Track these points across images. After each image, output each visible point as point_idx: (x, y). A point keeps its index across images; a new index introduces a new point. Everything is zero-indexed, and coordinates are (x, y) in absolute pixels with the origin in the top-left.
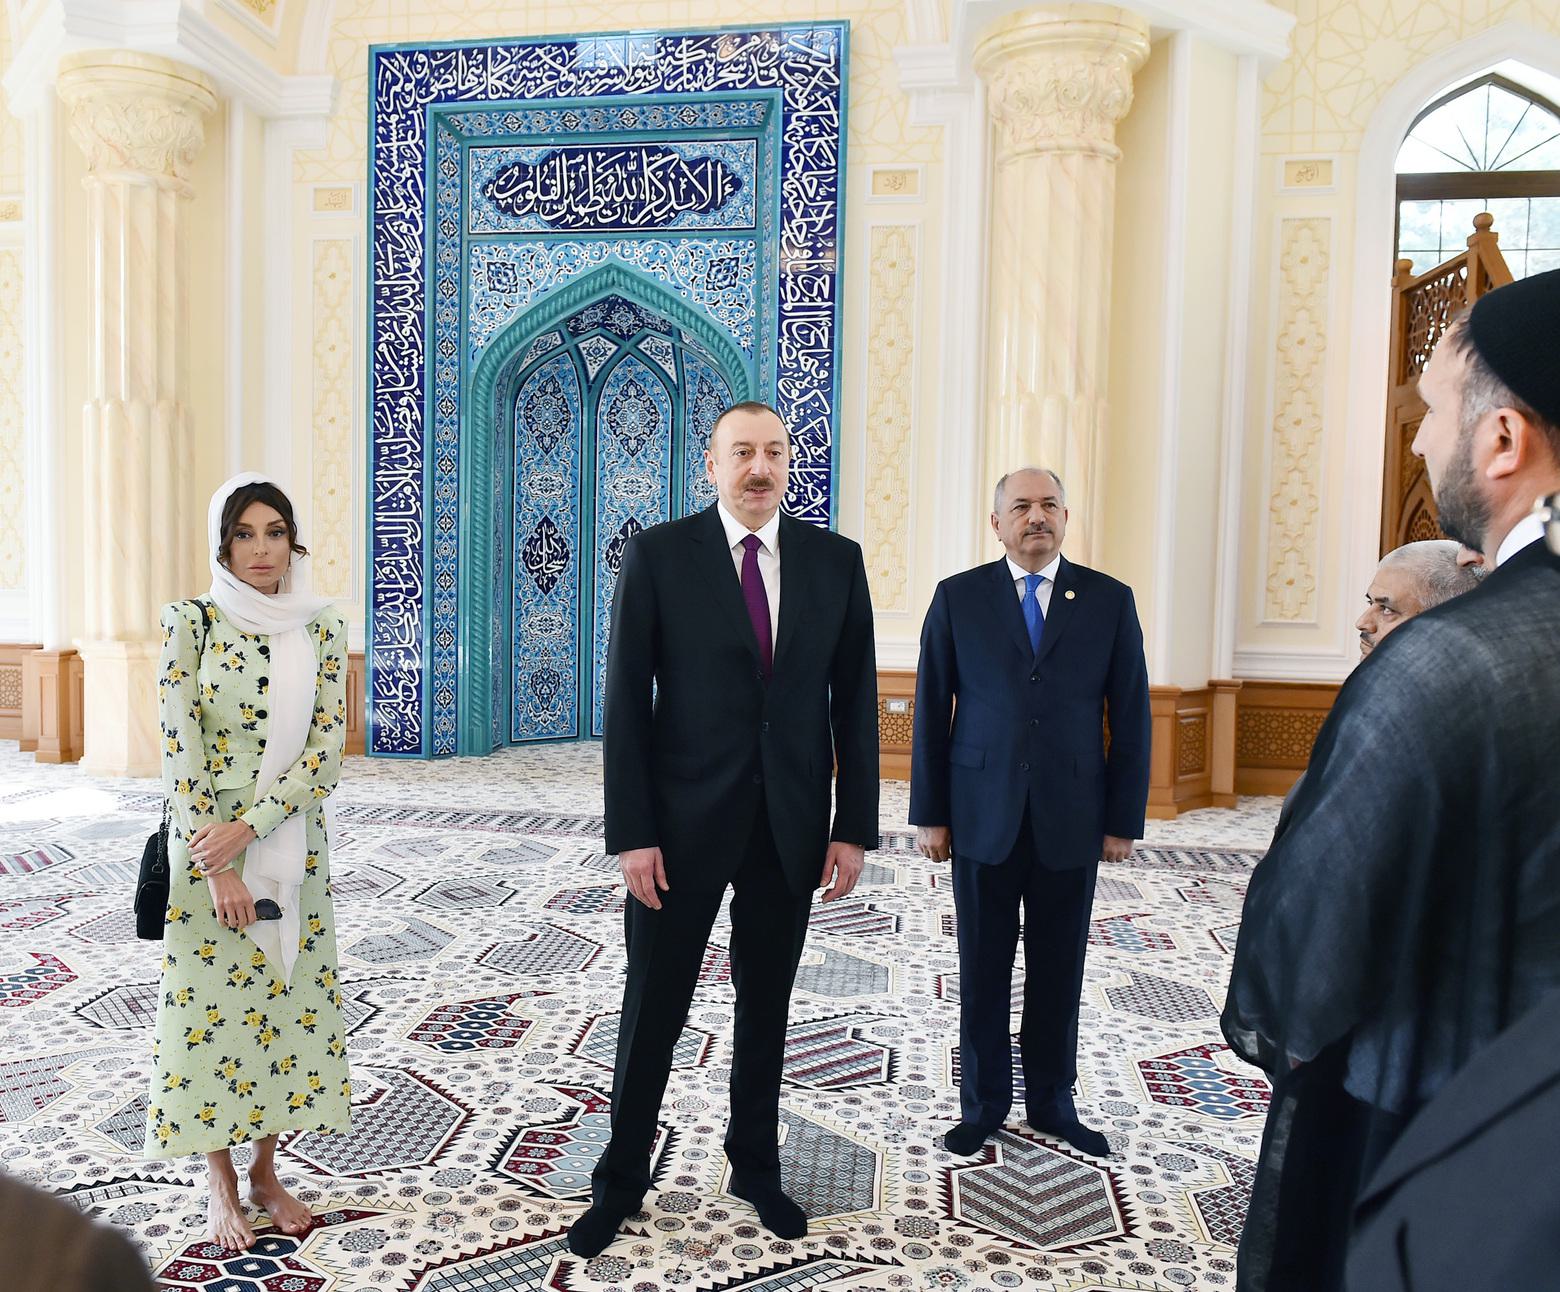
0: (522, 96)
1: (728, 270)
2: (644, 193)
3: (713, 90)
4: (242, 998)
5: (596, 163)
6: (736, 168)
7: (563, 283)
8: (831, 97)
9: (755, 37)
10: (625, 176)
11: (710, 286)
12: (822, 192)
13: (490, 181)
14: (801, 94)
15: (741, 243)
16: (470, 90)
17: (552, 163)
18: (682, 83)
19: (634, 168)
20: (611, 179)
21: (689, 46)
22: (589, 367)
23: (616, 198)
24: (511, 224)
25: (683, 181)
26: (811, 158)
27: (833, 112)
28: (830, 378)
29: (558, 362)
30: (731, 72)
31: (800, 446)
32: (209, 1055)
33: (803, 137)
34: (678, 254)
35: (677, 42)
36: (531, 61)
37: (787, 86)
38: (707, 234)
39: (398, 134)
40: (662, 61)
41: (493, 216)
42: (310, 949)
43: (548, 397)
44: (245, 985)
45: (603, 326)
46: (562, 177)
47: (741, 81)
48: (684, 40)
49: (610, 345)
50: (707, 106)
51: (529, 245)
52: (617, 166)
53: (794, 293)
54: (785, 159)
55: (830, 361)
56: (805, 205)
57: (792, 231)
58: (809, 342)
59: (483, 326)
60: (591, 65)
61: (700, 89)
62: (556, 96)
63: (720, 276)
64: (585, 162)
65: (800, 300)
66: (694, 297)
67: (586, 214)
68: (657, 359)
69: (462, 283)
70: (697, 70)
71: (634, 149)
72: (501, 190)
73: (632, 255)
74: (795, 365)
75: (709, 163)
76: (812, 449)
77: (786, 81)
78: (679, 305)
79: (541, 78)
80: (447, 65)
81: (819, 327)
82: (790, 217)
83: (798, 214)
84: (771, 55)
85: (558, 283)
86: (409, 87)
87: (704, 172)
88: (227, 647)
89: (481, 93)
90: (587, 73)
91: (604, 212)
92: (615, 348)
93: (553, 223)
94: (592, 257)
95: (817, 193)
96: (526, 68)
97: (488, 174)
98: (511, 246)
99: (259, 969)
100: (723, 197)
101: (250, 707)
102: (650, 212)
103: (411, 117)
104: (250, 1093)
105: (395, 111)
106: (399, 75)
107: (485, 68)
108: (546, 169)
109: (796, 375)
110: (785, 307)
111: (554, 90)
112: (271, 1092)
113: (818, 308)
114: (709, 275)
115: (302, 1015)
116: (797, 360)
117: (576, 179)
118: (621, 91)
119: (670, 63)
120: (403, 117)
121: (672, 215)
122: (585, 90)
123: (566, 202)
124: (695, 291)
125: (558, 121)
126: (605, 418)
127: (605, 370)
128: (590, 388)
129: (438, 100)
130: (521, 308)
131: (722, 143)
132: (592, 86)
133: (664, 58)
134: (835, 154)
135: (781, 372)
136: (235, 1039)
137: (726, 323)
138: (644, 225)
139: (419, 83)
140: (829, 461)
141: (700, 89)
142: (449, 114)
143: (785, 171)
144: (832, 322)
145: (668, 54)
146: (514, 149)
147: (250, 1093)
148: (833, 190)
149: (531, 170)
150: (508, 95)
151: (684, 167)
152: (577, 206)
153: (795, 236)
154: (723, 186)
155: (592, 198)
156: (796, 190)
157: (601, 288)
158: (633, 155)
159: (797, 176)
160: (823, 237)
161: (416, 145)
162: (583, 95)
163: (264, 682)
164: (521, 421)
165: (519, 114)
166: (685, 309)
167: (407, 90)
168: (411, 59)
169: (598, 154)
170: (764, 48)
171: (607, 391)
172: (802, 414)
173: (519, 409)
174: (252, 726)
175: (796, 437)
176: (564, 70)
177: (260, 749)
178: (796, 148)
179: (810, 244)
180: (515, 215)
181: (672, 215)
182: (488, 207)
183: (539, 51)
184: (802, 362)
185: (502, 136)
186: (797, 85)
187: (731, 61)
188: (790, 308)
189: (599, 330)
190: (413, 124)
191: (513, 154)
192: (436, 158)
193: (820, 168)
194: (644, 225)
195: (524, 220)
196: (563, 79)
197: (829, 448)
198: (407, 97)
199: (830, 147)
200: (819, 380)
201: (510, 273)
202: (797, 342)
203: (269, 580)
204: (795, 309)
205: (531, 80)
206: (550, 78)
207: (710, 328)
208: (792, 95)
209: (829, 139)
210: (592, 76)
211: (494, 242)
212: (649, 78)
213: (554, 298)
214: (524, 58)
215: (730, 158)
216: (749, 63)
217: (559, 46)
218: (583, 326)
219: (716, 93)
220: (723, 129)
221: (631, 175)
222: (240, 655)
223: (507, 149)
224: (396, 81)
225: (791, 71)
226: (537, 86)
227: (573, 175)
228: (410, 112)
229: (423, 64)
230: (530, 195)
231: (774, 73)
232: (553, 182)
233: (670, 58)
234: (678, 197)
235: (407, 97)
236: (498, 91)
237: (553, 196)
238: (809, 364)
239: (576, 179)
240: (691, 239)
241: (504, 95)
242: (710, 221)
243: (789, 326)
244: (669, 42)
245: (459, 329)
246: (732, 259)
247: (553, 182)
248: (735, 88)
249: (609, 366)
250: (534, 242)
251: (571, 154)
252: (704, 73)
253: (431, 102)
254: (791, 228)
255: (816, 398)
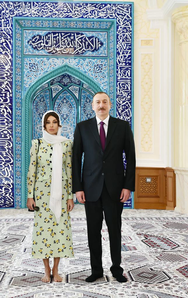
0: (42, 16)
1: (100, 67)
2: (76, 45)
3: (97, 18)
4: (46, 226)
5: (62, 36)
6: (102, 39)
7: (52, 70)
8: (130, 22)
9: (108, 5)
10: (70, 40)
11: (95, 72)
12: (127, 48)
13: (30, 40)
14: (121, 21)
15: (103, 60)
16: (26, 14)
17: (49, 35)
18: (88, 16)
19: (73, 38)
20: (66, 41)
21: (90, 6)
22: (53, 94)
23: (68, 46)
24: (36, 52)
25: (87, 43)
26: (124, 38)
27: (130, 26)
28: (131, 98)
29: (45, 92)
30: (102, 14)
31: (123, 116)
32: (41, 238)
33: (122, 33)
34: (85, 63)
35: (87, 4)
36: (44, 7)
37: (117, 18)
38: (94, 57)
39: (4, 25)
40: (83, 9)
41: (31, 50)
42: (62, 216)
43: (42, 102)
44: (48, 222)
45: (60, 82)
46: (52, 40)
47: (105, 16)
48: (89, 4)
49: (60, 88)
50: (95, 22)
51: (42, 59)
52: (68, 37)
53: (120, 75)
54: (117, 38)
55: (130, 93)
56: (123, 51)
57: (120, 58)
58: (125, 88)
59: (28, 81)
60: (62, 9)
61: (93, 18)
62: (52, 17)
63: (97, 69)
64: (58, 36)
65: (122, 77)
66: (90, 75)
67: (59, 51)
68: (73, 92)
69: (22, 69)
70: (93, 13)
71: (73, 33)
72: (33, 42)
73: (72, 62)
74: (121, 94)
75: (94, 38)
76: (126, 117)
77: (117, 17)
78: (86, 77)
79: (47, 12)
80: (19, 6)
81: (127, 84)
82: (119, 54)
83: (121, 53)
84: (113, 10)
85: (51, 70)
86: (7, 11)
87: (92, 41)
88: (44, 148)
89: (30, 15)
90: (61, 11)
91: (64, 50)
92: (62, 88)
93: (49, 53)
94: (60, 63)
95: (126, 48)
96: (43, 8)
97: (30, 38)
98: (36, 58)
99: (51, 219)
100: (98, 48)
101: (48, 160)
102: (77, 51)
103: (8, 20)
104: (50, 247)
105: (3, 18)
106: (4, 8)
107: (31, 8)
108: (47, 37)
109: (121, 97)
110: (118, 78)
111: (51, 16)
112: (55, 247)
113: (127, 79)
114: (94, 69)
115: (61, 231)
116: (122, 93)
117: (56, 40)
118: (71, 17)
119: (85, 10)
120: (6, 20)
121: (84, 52)
122: (60, 16)
123: (53, 47)
124: (90, 73)
125: (52, 24)
126: (57, 109)
127: (57, 95)
128: (52, 100)
129: (16, 16)
130: (40, 76)
131: (97, 33)
132: (62, 15)
133: (83, 8)
134: (131, 37)
135: (117, 96)
136: (46, 234)
137: (99, 82)
138: (76, 54)
139: (10, 11)
140: (131, 121)
141: (93, 18)
142: (19, 20)
143: (117, 42)
144: (131, 83)
145: (84, 7)
146: (37, 31)
147: (50, 247)
148: (130, 47)
149: (42, 37)
150: (38, 16)
151: (87, 39)
152: (56, 48)
153: (120, 59)
154: (98, 44)
155: (61, 46)
156: (120, 47)
157: (63, 71)
158: (72, 34)
159: (121, 43)
160: (128, 60)
161: (10, 28)
162: (60, 17)
163: (51, 155)
164: (35, 109)
165: (40, 21)
166: (87, 78)
167: (7, 12)
168: (8, 4)
169: (62, 34)
170: (111, 8)
171: (57, 101)
172: (123, 108)
173: (34, 106)
174: (49, 165)
175: (122, 114)
176: (54, 10)
177: (51, 170)
178: (120, 35)
179: (125, 61)
180: (38, 50)
181: (84, 52)
182: (30, 47)
183: (47, 4)
184: (123, 94)
185: (34, 27)
186: (120, 19)
187: (102, 11)
188: (119, 79)
189: (58, 83)
190: (9, 22)
191: (37, 32)
192: (16, 33)
193: (127, 41)
194: (75, 54)
195: (41, 51)
196: (54, 13)
197: (131, 117)
198: (7, 14)
199: (129, 36)
200: (128, 99)
201: (36, 66)
202: (122, 88)
203: (55, 132)
204: (121, 79)
205: (45, 12)
206: (50, 12)
207: (94, 84)
208: (119, 21)
209: (129, 33)
210: (62, 12)
211: (31, 57)
212: (79, 14)
213: (50, 74)
214: (42, 6)
215: (100, 37)
216: (107, 12)
217: (53, 3)
218: (54, 82)
219: (98, 19)
220: (98, 29)
221: (72, 40)
222: (46, 150)
223: (35, 31)
224: (3, 10)
225: (118, 15)
226: (46, 14)
227: (55, 39)
228: (8, 19)
229: (12, 5)
230: (42, 44)
231: (114, 15)
232: (49, 41)
233: (85, 9)
234: (85, 47)
235: (7, 14)
236: (35, 14)
237: (49, 45)
238: (125, 94)
239: (56, 40)
240: (89, 59)
241: (37, 16)
242: (95, 54)
243: (119, 84)
244: (84, 4)
245: (21, 82)
246: (101, 65)
247: (49, 41)
248: (103, 18)
249: (59, 94)
250: (43, 58)
251: (54, 33)
252: (95, 13)
253: (15, 16)
254: (119, 57)
255: (127, 103)
